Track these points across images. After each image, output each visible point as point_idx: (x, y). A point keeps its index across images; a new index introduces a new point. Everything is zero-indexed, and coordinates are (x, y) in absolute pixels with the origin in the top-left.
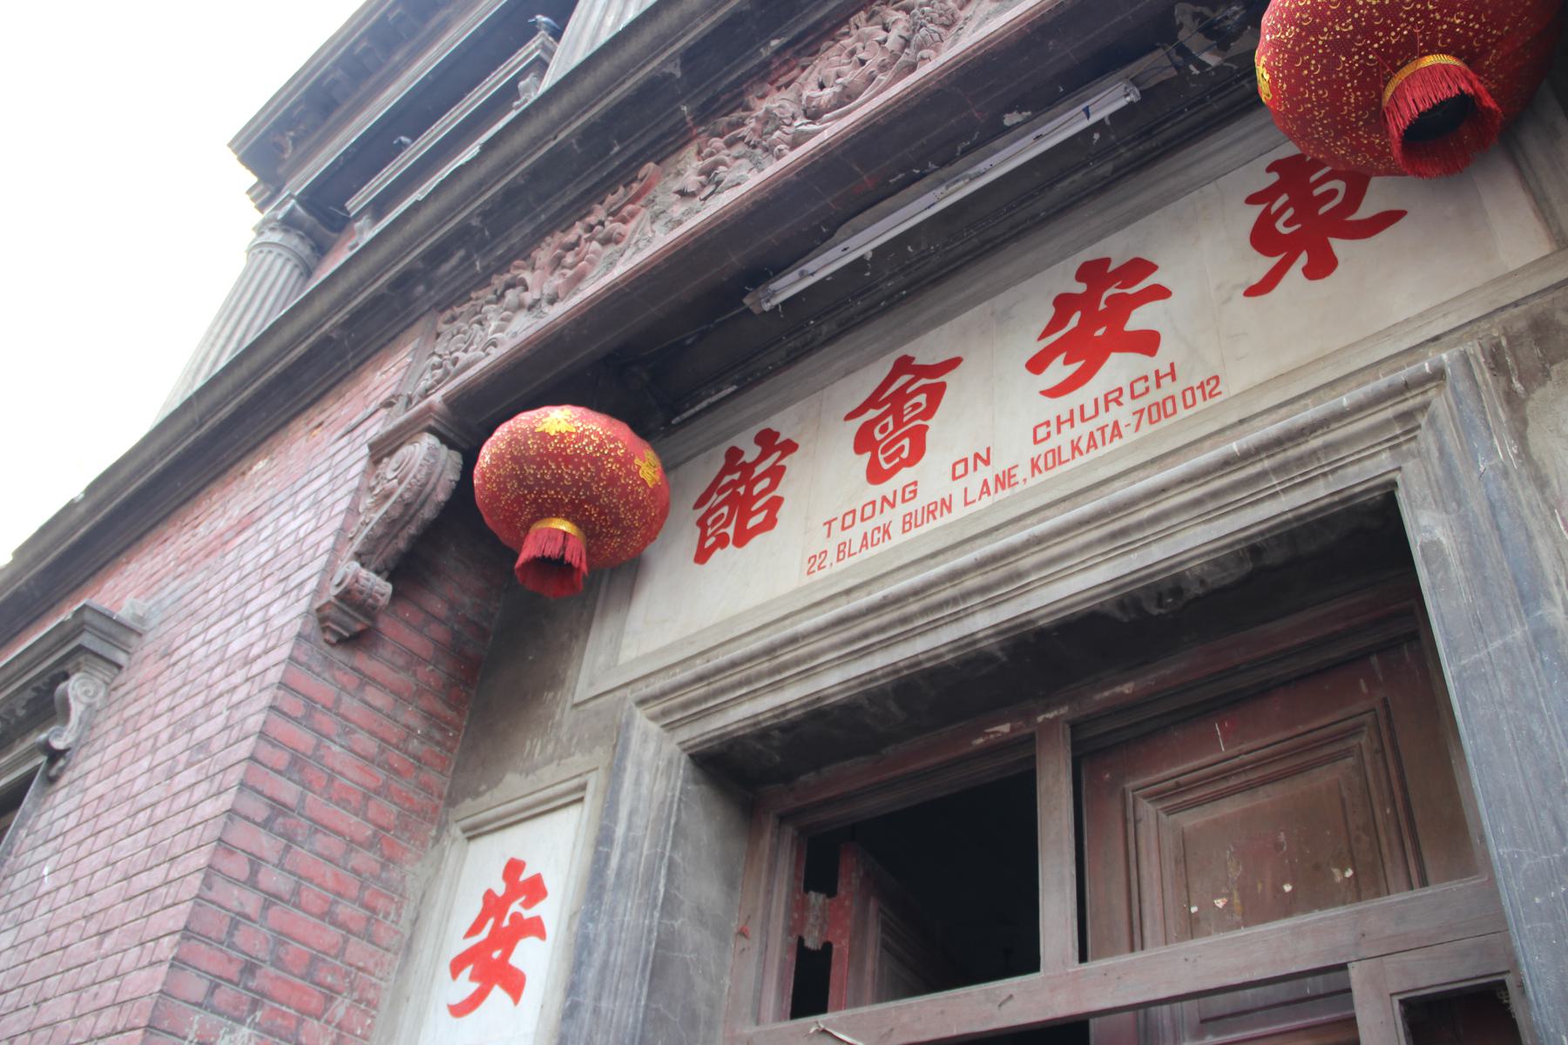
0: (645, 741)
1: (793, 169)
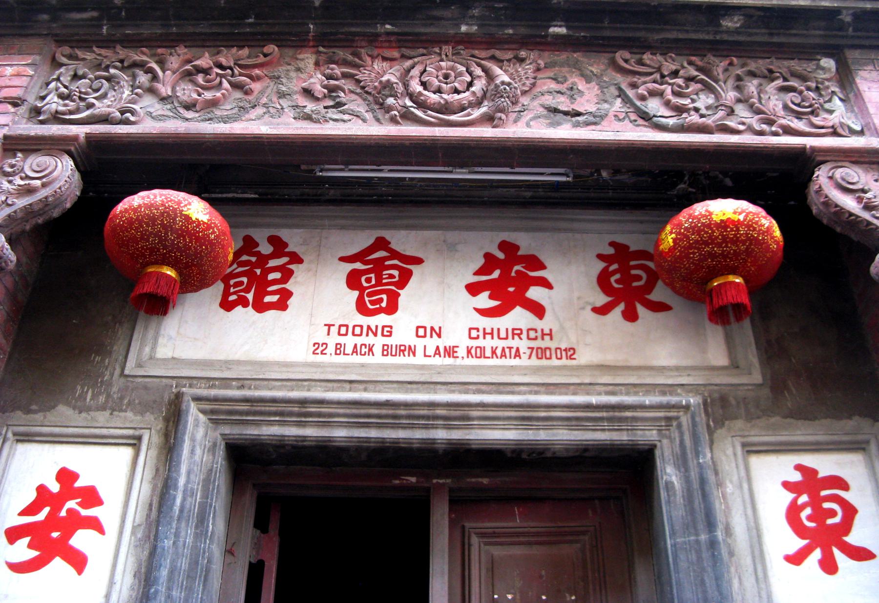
1: (410, 140)
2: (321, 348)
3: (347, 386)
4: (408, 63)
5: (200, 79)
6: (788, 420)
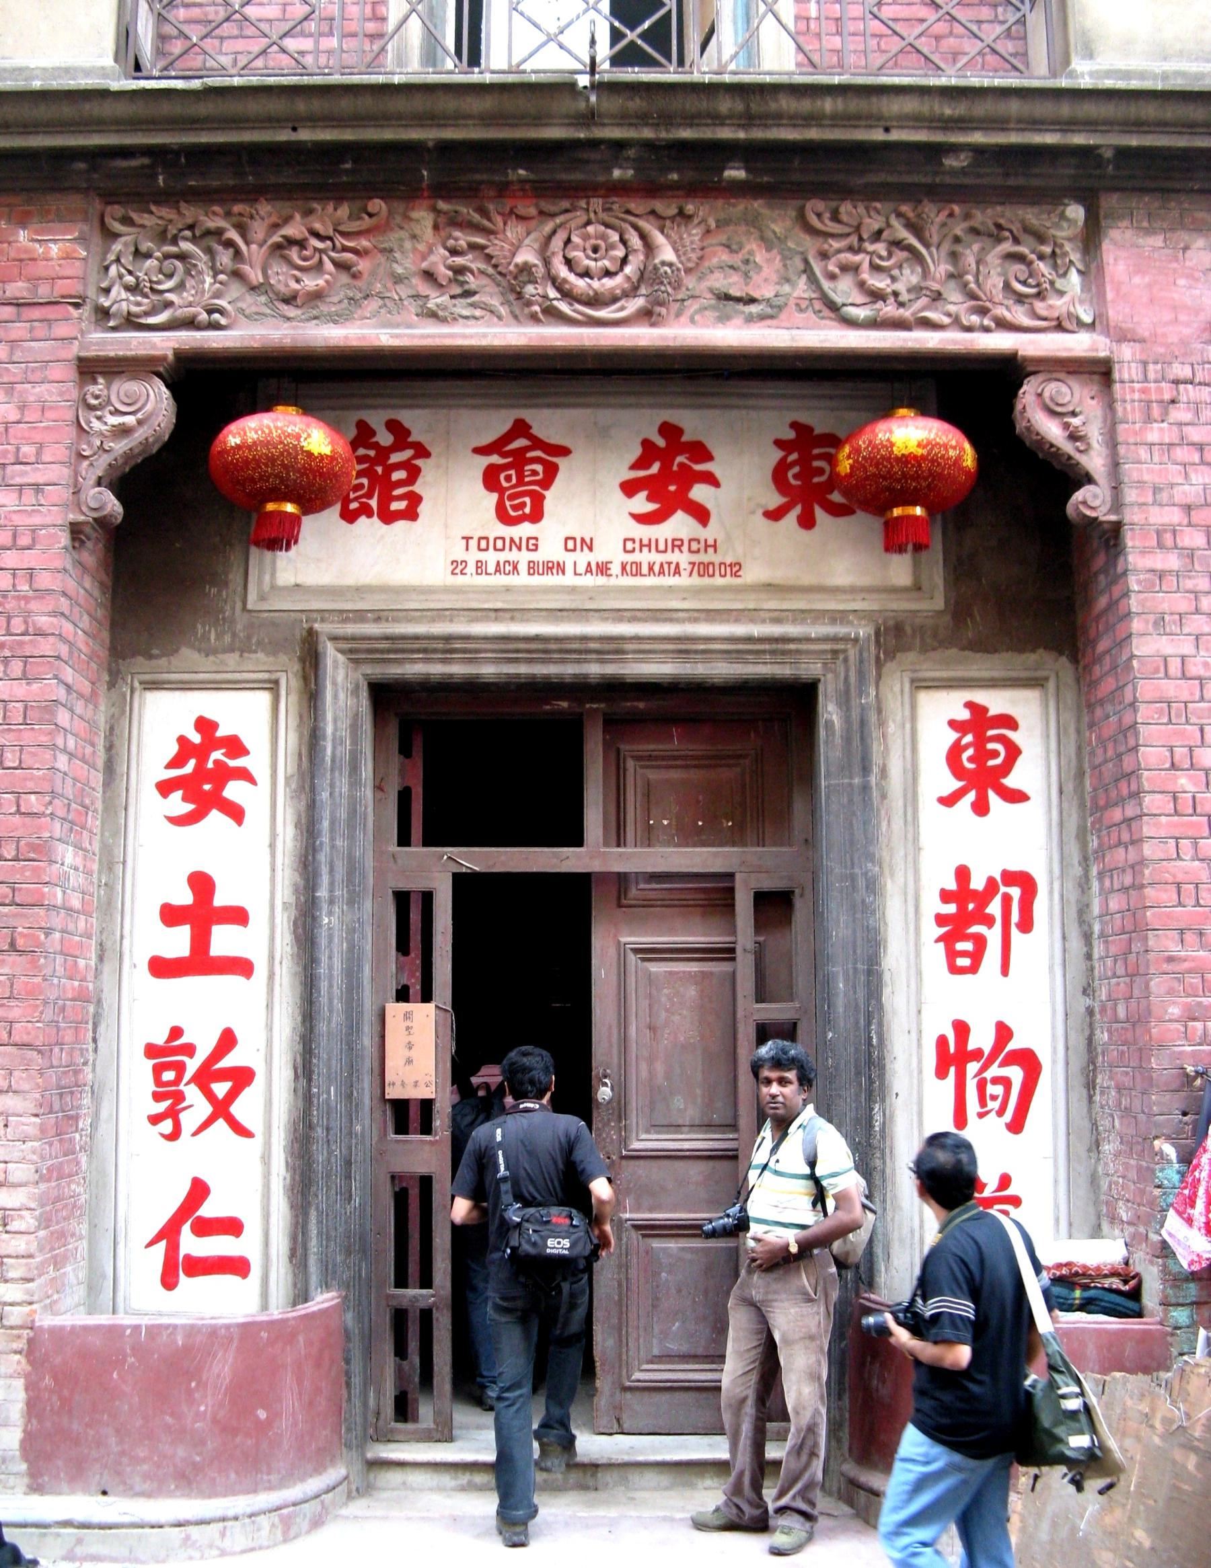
0: (336, 667)
2: (460, 567)
3: (493, 614)
4: (548, 227)
5: (294, 253)
6: (967, 653)
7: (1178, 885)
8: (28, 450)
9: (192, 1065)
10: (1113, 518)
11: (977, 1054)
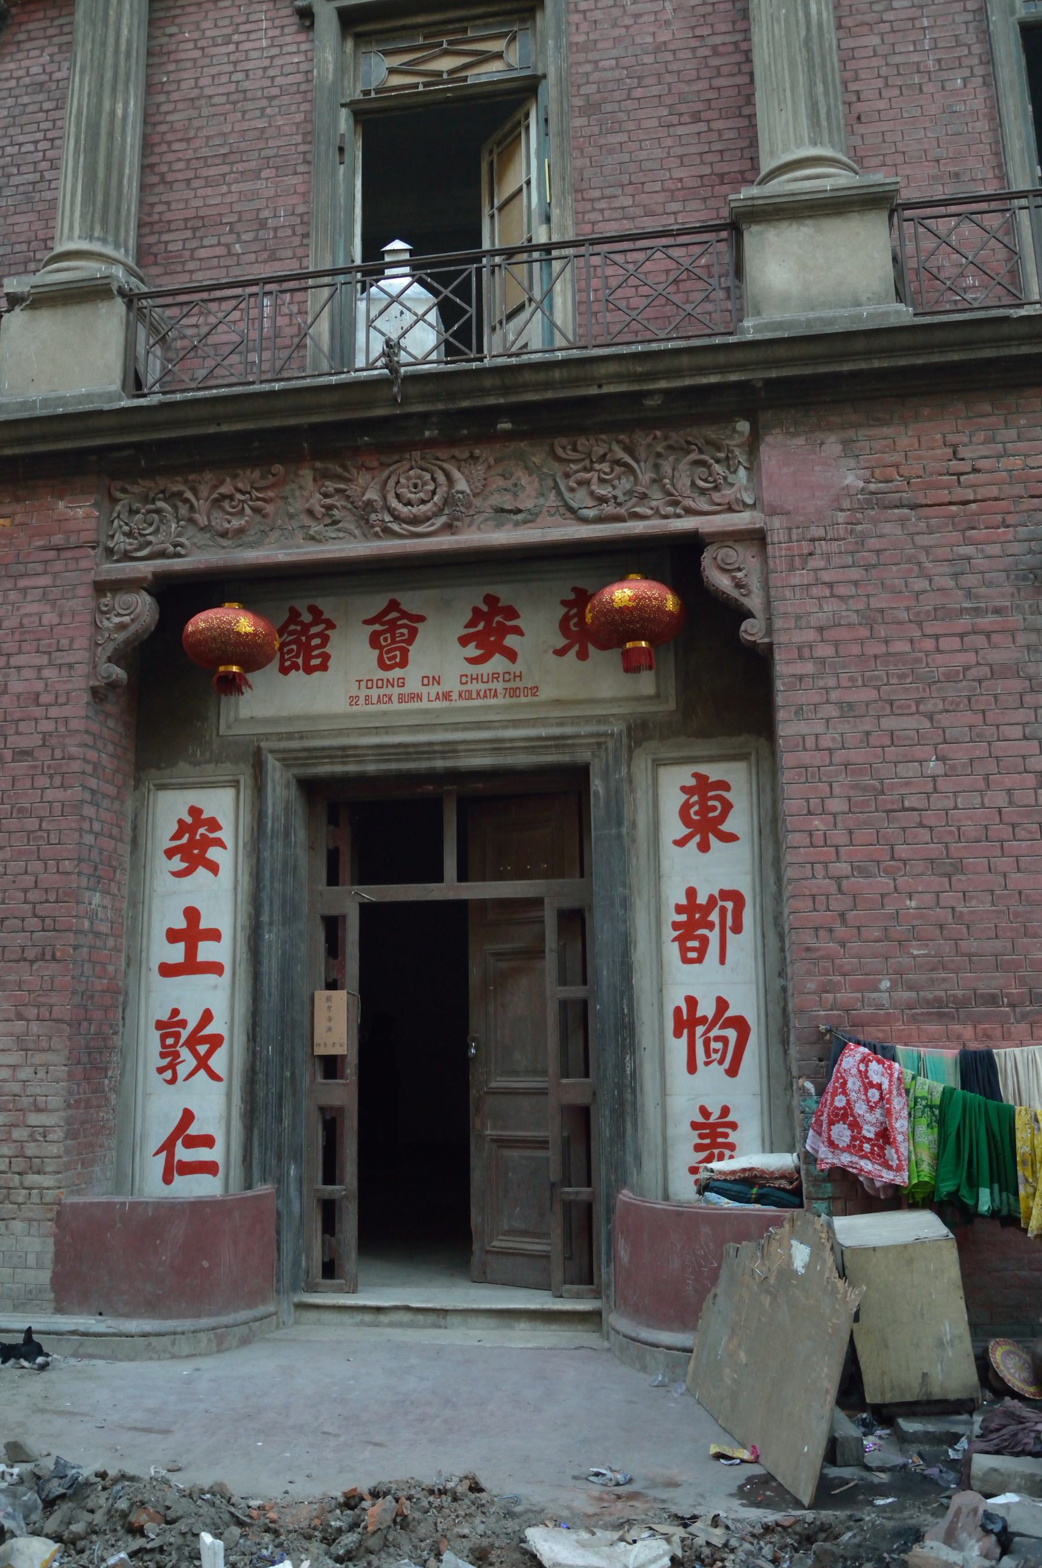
0: (274, 770)
4: (386, 473)
5: (226, 504)
7: (814, 897)
8: (65, 642)
9: (185, 1034)
10: (766, 640)
11: (703, 1020)
